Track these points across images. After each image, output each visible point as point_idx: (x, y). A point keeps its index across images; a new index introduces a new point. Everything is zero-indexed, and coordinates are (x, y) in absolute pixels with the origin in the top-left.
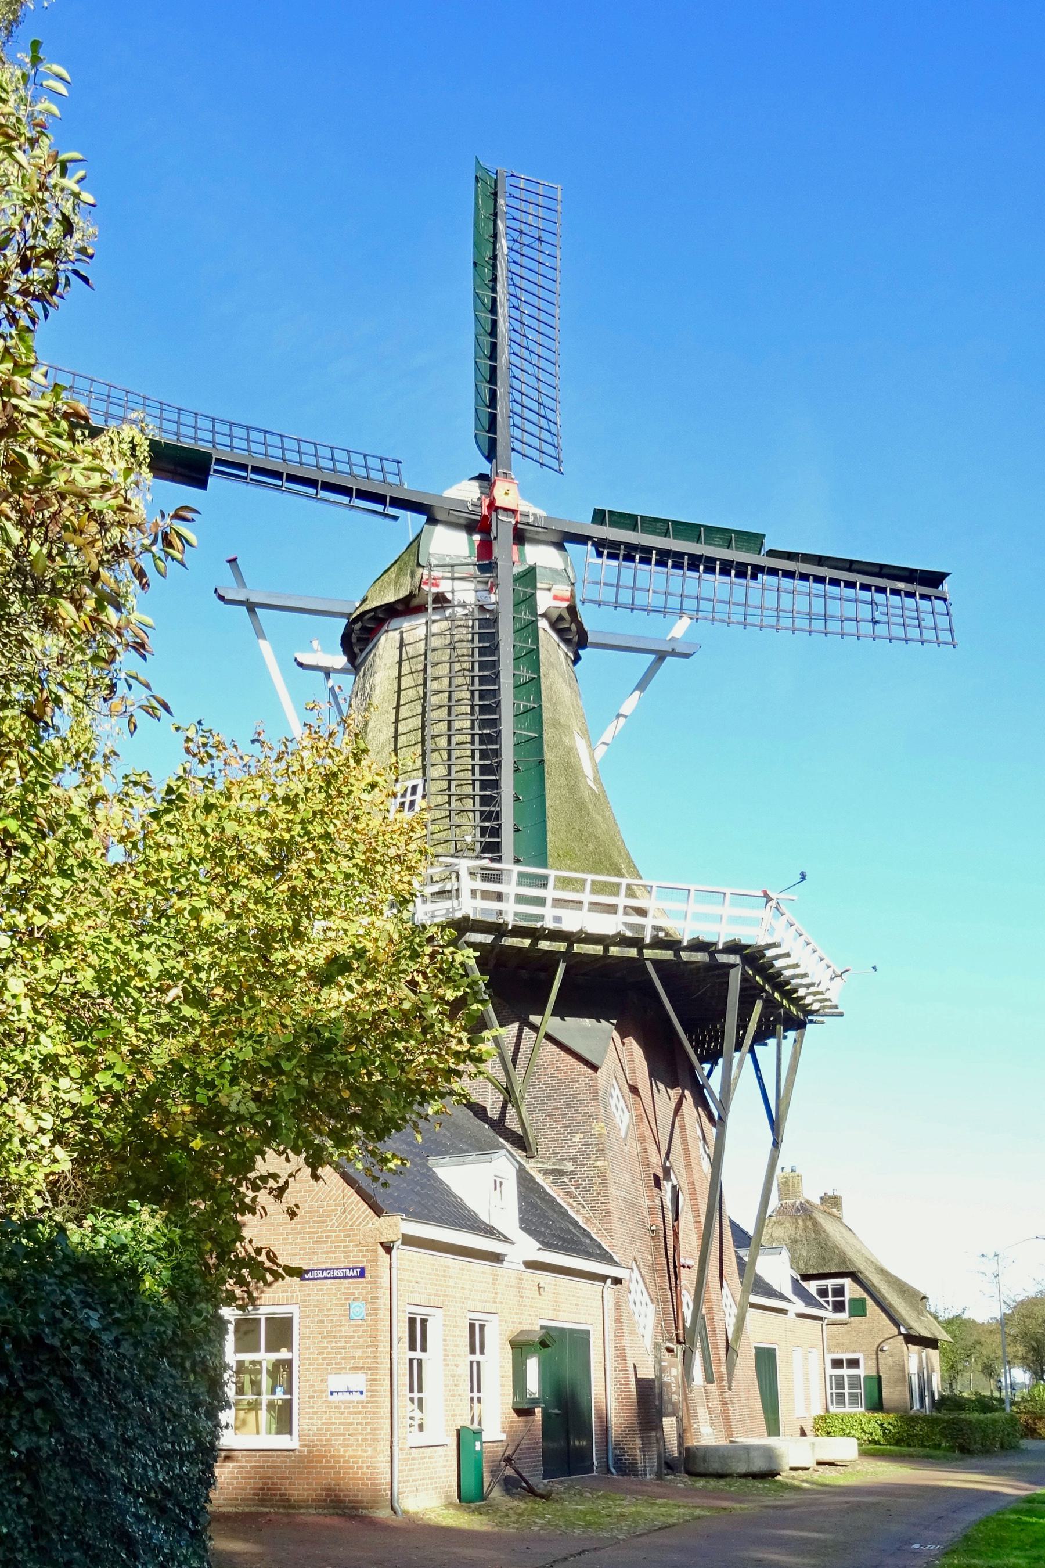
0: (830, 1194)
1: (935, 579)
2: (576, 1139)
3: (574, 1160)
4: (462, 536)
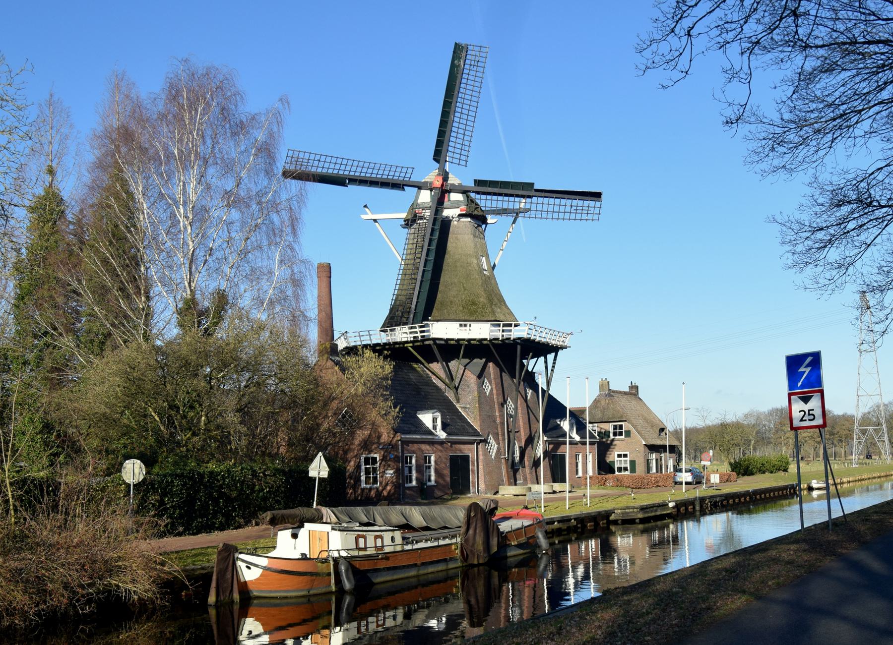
1: (597, 196)
3: (469, 404)
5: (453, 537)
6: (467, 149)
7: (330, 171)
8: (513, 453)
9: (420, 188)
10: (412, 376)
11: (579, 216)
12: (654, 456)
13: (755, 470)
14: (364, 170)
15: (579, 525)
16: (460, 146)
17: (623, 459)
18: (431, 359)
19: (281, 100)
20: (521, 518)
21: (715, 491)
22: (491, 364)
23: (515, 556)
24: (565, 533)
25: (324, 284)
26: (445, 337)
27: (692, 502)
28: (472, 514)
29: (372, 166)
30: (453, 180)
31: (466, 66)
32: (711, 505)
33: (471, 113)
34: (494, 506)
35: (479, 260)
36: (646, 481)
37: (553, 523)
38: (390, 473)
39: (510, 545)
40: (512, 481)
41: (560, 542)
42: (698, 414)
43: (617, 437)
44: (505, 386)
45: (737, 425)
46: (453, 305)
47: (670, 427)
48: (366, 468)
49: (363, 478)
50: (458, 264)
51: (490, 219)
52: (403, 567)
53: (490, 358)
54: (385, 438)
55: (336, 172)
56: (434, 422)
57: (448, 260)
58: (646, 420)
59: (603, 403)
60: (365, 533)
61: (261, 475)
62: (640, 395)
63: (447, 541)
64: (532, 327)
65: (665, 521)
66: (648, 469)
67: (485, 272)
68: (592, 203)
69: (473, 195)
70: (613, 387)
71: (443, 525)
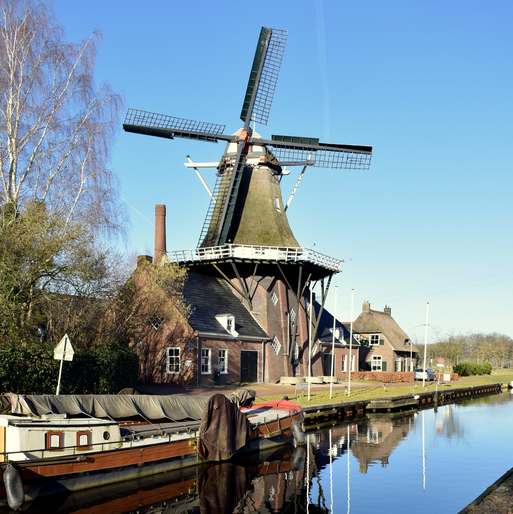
1: (368, 149)
3: (260, 312)
4: (261, 147)
5: (194, 430)
6: (267, 111)
7: (160, 126)
8: (294, 352)
9: (229, 141)
10: (217, 289)
11: (353, 166)
12: (400, 359)
13: (469, 373)
14: (187, 126)
15: (340, 413)
16: (262, 109)
17: (377, 360)
18: (232, 276)
19: (95, 32)
20: (280, 409)
21: (446, 387)
22: (279, 282)
23: (267, 449)
24: (327, 419)
25: (161, 221)
26: (242, 257)
27: (431, 395)
28: (215, 406)
29: (193, 123)
30: (256, 135)
31: (270, 46)
32: (444, 398)
33: (272, 83)
34: (251, 397)
35: (273, 200)
36: (394, 377)
37: (316, 411)
38: (189, 363)
39: (261, 439)
40: (292, 373)
41: (321, 428)
42: (433, 330)
43: (375, 345)
44: (289, 299)
45: (462, 340)
46: (251, 233)
47: (413, 340)
48: (170, 358)
49: (168, 365)
50: (257, 202)
51: (285, 170)
52: (117, 469)
53: (278, 277)
54: (186, 333)
55: (164, 127)
56: (228, 324)
57: (250, 198)
58: (395, 333)
59: (365, 319)
60: (61, 429)
61: (36, 357)
62: (392, 315)
63: (185, 436)
64: (312, 252)
65: (411, 411)
66: (396, 369)
67: (278, 210)
68: (364, 156)
69: (270, 148)
70: (372, 308)
71: (187, 416)
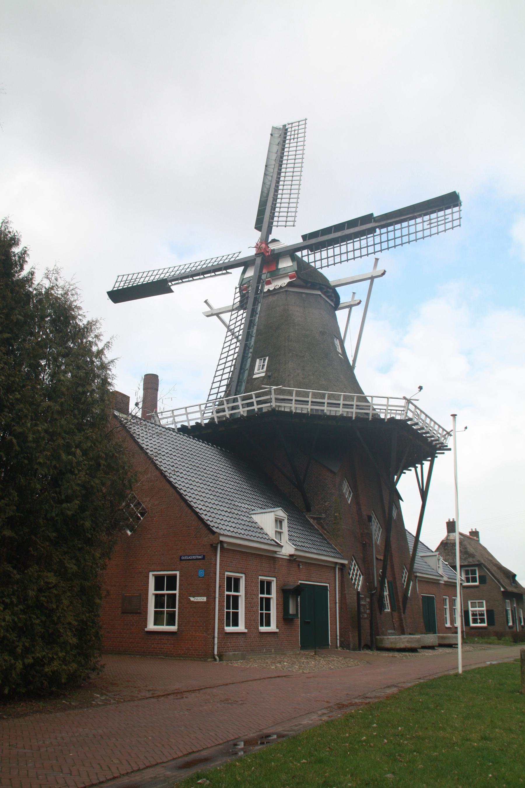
0: (474, 530)
2: (326, 504)
